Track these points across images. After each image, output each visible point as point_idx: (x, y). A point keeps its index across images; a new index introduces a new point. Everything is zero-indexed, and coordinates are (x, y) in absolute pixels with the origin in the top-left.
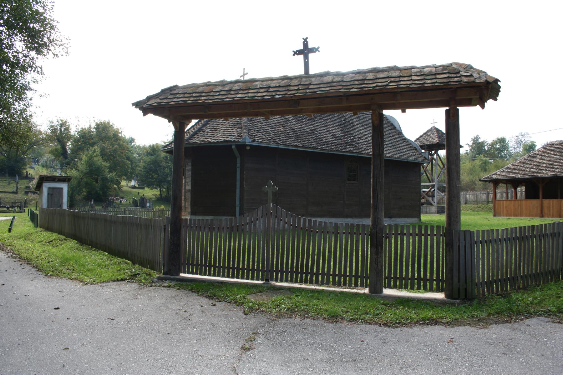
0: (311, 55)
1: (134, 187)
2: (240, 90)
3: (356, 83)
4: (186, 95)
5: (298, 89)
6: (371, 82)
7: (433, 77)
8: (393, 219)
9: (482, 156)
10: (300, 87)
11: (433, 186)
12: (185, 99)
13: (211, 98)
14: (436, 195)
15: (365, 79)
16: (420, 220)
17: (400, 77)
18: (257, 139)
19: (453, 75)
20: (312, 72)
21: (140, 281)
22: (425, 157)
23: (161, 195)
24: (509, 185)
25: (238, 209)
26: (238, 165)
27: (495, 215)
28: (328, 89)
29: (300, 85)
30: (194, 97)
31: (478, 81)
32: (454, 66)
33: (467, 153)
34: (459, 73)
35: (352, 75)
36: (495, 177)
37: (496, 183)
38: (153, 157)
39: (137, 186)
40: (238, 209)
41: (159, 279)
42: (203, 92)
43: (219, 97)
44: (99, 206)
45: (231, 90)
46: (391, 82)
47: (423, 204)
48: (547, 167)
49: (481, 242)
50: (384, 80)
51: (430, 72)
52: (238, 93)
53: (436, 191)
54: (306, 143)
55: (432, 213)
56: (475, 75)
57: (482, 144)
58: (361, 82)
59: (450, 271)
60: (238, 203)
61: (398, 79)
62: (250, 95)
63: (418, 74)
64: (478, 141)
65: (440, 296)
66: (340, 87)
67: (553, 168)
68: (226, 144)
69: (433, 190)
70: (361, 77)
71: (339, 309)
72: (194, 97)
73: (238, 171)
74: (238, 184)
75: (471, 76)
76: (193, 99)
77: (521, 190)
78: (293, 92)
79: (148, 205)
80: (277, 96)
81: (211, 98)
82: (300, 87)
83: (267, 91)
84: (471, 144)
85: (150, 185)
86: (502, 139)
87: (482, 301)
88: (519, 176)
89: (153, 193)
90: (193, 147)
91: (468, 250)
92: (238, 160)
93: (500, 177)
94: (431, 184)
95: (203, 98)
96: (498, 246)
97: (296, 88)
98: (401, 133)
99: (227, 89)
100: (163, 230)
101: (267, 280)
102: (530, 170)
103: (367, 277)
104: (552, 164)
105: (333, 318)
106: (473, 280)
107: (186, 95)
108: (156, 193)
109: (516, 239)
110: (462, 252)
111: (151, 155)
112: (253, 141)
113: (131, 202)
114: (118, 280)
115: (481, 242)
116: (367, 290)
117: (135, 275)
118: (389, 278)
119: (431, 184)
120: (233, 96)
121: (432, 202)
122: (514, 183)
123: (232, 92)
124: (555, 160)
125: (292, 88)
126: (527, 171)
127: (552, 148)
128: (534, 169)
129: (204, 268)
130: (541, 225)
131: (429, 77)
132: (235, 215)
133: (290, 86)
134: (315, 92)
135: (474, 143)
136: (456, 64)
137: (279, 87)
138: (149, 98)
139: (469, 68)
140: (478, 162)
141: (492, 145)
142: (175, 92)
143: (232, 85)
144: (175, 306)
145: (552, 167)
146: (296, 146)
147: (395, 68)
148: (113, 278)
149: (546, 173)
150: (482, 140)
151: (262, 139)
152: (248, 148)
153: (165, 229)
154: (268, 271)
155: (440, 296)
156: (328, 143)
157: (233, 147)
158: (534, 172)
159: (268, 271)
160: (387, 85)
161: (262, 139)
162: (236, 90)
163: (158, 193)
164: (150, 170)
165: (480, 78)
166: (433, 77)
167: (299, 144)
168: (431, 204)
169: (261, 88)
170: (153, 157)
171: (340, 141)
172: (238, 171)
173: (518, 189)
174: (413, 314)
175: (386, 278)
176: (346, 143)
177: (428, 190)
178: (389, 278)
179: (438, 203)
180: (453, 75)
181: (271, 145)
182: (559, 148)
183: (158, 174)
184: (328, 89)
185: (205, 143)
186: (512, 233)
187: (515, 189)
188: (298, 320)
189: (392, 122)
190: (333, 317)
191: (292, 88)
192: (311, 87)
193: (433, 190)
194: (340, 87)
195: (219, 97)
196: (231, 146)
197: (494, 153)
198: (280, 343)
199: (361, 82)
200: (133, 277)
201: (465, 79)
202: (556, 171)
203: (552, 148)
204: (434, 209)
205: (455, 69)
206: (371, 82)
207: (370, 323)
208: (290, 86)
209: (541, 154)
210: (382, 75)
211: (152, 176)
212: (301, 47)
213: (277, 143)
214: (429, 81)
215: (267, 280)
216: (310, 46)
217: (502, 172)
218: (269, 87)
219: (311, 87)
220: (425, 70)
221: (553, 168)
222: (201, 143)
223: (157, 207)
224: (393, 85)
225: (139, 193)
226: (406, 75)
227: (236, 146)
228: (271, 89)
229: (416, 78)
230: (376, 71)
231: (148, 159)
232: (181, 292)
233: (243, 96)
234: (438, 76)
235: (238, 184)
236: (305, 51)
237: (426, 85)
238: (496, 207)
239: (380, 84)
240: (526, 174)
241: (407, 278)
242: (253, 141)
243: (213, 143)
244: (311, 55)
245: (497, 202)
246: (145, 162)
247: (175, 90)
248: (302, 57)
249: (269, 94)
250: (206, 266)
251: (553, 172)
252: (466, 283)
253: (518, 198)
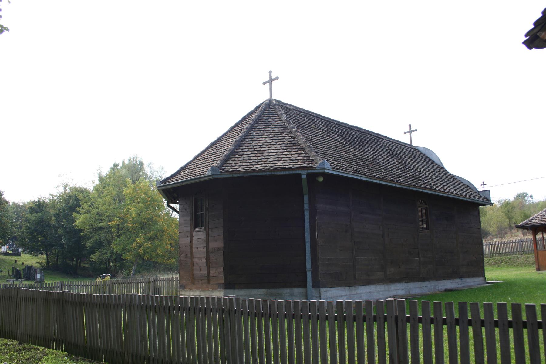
1: (6, 254)
8: (464, 280)
16: (485, 278)
23: (48, 262)
26: (306, 206)
27: (538, 269)
36: (535, 222)
38: (40, 214)
39: (11, 252)
40: (309, 275)
44: (507, 286)
60: (309, 266)
68: (291, 172)
79: (38, 276)
85: (33, 250)
89: (38, 261)
90: (233, 178)
92: (306, 198)
98: (443, 168)
108: (41, 261)
111: (37, 212)
113: (10, 273)
132: (305, 286)
157: (304, 176)
164: (35, 231)
170: (40, 214)
185: (254, 171)
189: (427, 155)
196: (300, 175)
211: (37, 239)
222: (246, 172)
225: (16, 261)
227: (308, 175)
231: (33, 217)
238: (540, 259)
243: (268, 170)
246: (27, 220)
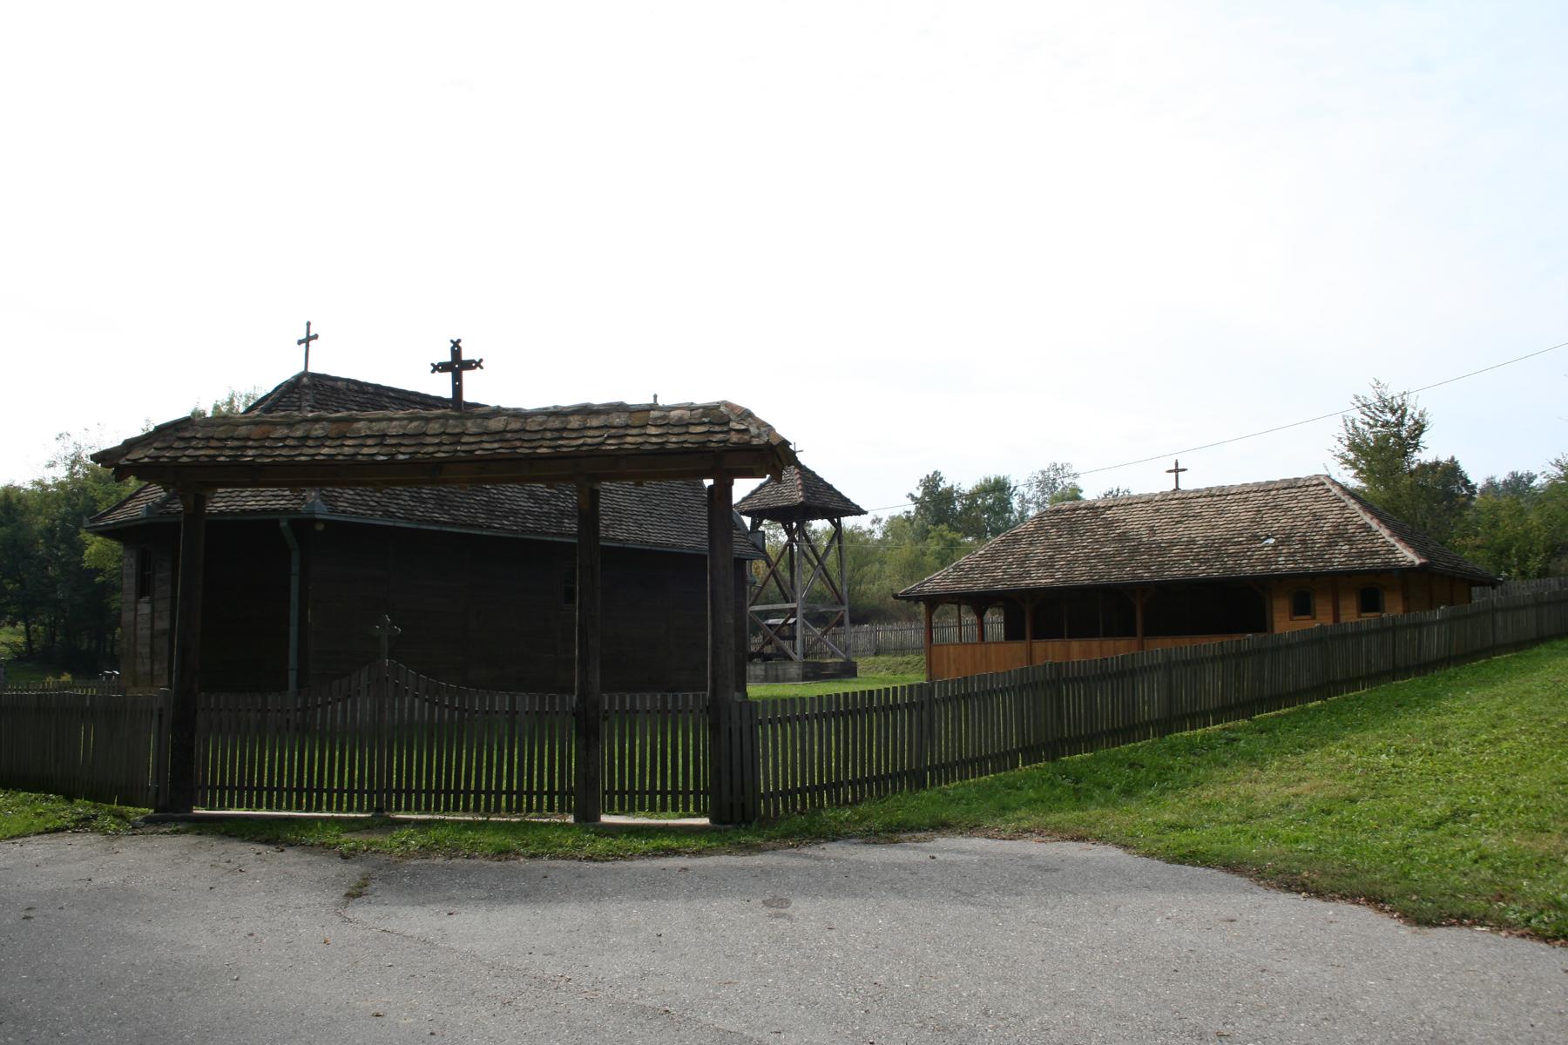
0: (466, 374)
2: (327, 437)
3: (548, 435)
4: (214, 443)
5: (440, 444)
6: (574, 435)
7: (683, 430)
9: (944, 527)
10: (445, 439)
11: (793, 613)
12: (211, 452)
13: (268, 452)
14: (798, 635)
15: (565, 429)
17: (627, 426)
18: (342, 505)
19: (717, 429)
20: (468, 397)
21: (103, 831)
22: (754, 545)
23: (29, 643)
24: (964, 608)
25: (292, 676)
26: (295, 568)
28: (496, 445)
29: (444, 433)
30: (231, 448)
31: (755, 442)
32: (722, 409)
33: (908, 518)
34: (727, 423)
35: (540, 419)
37: (932, 601)
40: (292, 676)
41: (149, 821)
42: (249, 439)
43: (284, 452)
45: (307, 437)
46: (609, 437)
47: (752, 656)
48: (1040, 564)
49: (770, 721)
50: (597, 433)
51: (680, 419)
52: (323, 446)
53: (798, 626)
54: (462, 514)
55: (791, 680)
56: (753, 430)
57: (949, 496)
58: (557, 434)
59: (716, 773)
61: (622, 432)
62: (346, 450)
63: (659, 422)
64: (937, 486)
65: (705, 821)
66: (518, 444)
67: (1052, 567)
69: (791, 621)
70: (557, 424)
71: (511, 841)
72: (231, 448)
73: (295, 582)
74: (294, 615)
75: (746, 431)
76: (228, 452)
77: (995, 621)
78: (431, 449)
80: (401, 457)
81: (268, 452)
82: (445, 439)
83: (381, 445)
84: (918, 494)
86: (997, 482)
87: (768, 822)
88: (980, 585)
91: (746, 737)
92: (295, 558)
93: (939, 589)
94: (787, 606)
95: (250, 452)
96: (803, 728)
97: (437, 440)
99: (299, 433)
100: (156, 718)
101: (379, 810)
102: (1005, 572)
103: (571, 792)
104: (1051, 557)
105: (503, 853)
106: (756, 787)
107: (214, 443)
108: (14, 638)
109: (837, 715)
110: (736, 739)
112: (333, 510)
114: (48, 831)
115: (770, 721)
116: (570, 819)
117: (87, 819)
118: (611, 792)
119: (787, 606)
120: (312, 451)
121: (790, 652)
122: (979, 602)
123: (310, 443)
124: (1058, 548)
125: (429, 440)
126: (999, 574)
127: (1055, 519)
128: (1014, 570)
129: (247, 792)
130: (887, 690)
131: (676, 430)
133: (425, 434)
134: (472, 452)
135: (925, 494)
136: (727, 404)
137: (404, 435)
138: (130, 445)
139: (747, 415)
140: (934, 546)
141: (972, 496)
142: (187, 435)
143: (308, 426)
144: (205, 857)
145: (1049, 564)
146: (437, 522)
147: (620, 408)
148: (33, 829)
149: (1039, 578)
150: (948, 485)
151: (354, 504)
152: (320, 527)
153: (160, 716)
154: (380, 792)
155: (705, 821)
156: (515, 513)
157: (283, 524)
158: (1012, 577)
159: (380, 792)
160: (603, 443)
161: (354, 504)
162: (317, 438)
163: (21, 639)
165: (759, 436)
166: (683, 430)
167: (445, 518)
168: (791, 659)
169: (368, 436)
171: (546, 508)
172: (295, 582)
173: (988, 616)
174: (642, 845)
175: (605, 793)
176: (562, 513)
177: (781, 621)
178: (611, 792)
179: (805, 656)
180: (717, 429)
181: (378, 519)
182: (1068, 520)
183: (21, 581)
184: (496, 445)
186: (829, 705)
187: (980, 615)
188: (440, 861)
190: (501, 852)
191: (429, 440)
192: (465, 439)
193: (791, 621)
194: (518, 444)
195: (284, 452)
196: (277, 522)
197: (977, 519)
198: (410, 886)
199: (557, 434)
200: (84, 824)
201: (734, 438)
202: (1058, 575)
203: (1055, 519)
204: (794, 669)
205: (723, 415)
206: (574, 435)
207: (565, 858)
208: (425, 434)
209: (1031, 534)
210: (595, 422)
212: (448, 358)
213: (392, 515)
214: (674, 439)
215: (379, 810)
216: (465, 357)
217: (946, 577)
218: (384, 436)
219: (465, 439)
220: (673, 413)
221: (1052, 567)
223: (50, 679)
224: (611, 445)
226: (637, 423)
228: (389, 441)
229: (653, 431)
230: (586, 411)
232: (202, 839)
233: (332, 451)
234: (692, 429)
235: (294, 615)
236: (457, 365)
237: (670, 446)
239: (589, 441)
240: (996, 581)
241: (642, 792)
242: (333, 510)
244: (466, 374)
245: (934, 649)
247: (186, 429)
248: (449, 375)
249: (384, 450)
250: (250, 789)
251: (1052, 576)
252: (743, 793)
253: (988, 638)
